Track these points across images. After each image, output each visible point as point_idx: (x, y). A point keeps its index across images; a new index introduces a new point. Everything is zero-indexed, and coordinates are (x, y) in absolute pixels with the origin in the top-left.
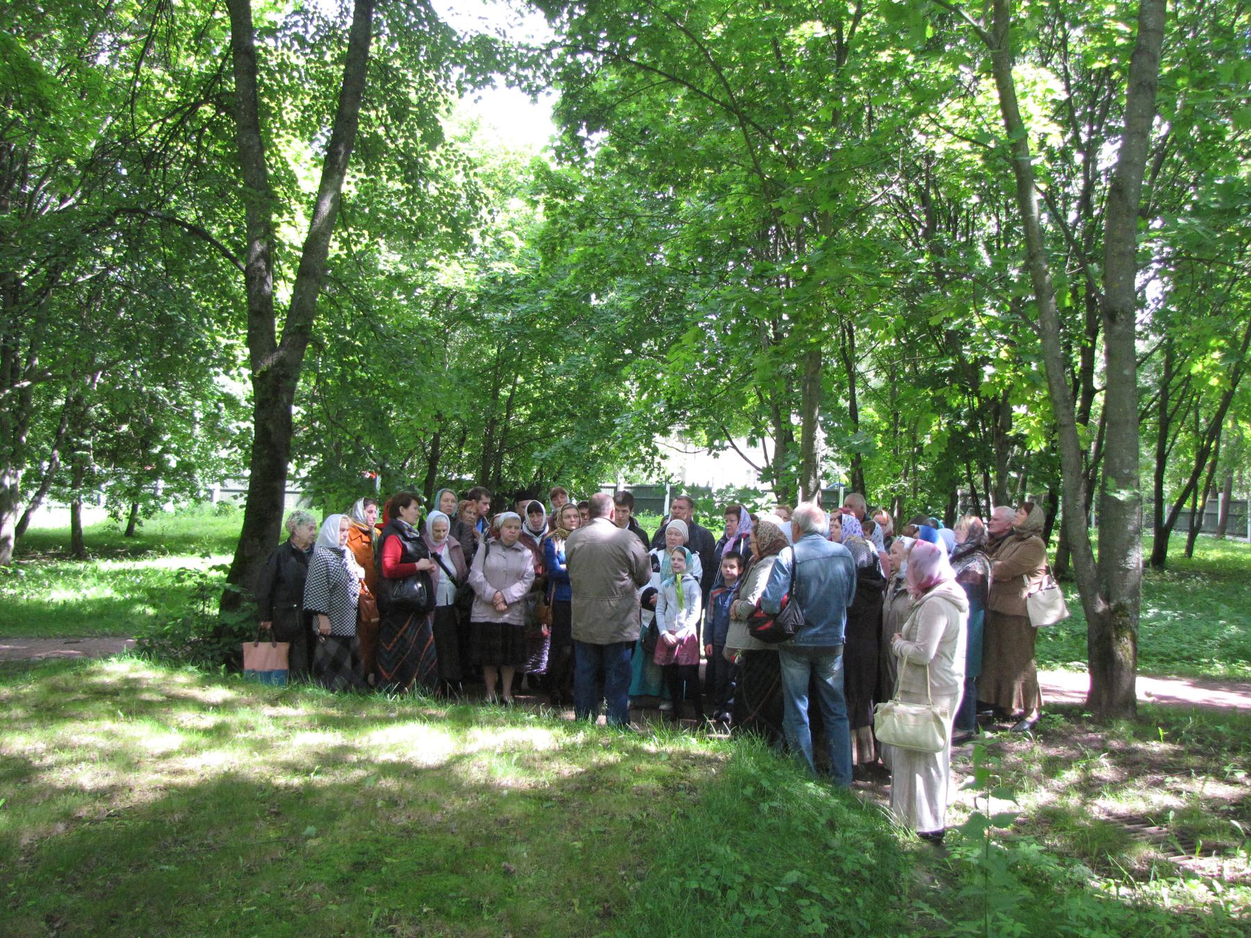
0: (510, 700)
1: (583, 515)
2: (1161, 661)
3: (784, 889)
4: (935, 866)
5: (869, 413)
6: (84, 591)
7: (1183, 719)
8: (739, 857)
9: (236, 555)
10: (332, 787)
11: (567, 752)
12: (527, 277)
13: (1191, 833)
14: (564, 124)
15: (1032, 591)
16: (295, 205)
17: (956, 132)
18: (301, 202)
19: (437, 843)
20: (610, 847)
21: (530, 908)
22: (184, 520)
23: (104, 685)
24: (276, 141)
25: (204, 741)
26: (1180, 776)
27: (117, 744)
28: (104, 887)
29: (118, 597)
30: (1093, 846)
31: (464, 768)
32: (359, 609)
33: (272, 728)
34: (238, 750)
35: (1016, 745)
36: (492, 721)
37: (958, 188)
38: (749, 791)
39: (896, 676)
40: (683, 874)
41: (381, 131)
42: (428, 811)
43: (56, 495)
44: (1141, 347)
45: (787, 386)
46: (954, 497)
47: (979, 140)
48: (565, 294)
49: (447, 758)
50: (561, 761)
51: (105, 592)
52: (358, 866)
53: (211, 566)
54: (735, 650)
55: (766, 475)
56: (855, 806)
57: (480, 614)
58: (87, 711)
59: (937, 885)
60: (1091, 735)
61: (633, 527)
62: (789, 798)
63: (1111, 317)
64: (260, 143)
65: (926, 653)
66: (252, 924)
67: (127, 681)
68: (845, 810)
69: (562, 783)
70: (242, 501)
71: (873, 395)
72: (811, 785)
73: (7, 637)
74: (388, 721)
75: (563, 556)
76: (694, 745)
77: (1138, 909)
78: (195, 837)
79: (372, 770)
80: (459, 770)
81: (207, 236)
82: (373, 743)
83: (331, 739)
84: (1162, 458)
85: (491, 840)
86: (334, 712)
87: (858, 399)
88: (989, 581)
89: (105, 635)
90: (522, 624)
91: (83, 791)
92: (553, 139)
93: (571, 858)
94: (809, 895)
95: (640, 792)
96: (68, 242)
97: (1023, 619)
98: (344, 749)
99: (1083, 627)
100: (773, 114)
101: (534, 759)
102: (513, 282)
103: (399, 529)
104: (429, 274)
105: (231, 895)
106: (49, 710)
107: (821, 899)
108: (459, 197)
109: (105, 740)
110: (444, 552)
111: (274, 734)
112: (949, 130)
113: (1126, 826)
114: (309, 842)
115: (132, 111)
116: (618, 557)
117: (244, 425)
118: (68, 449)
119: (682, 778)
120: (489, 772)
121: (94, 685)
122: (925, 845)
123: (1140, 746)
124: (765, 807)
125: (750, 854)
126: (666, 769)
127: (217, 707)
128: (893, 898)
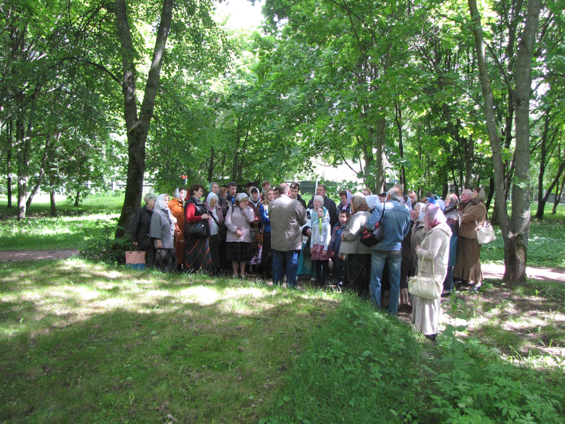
0: (243, 276)
1: (277, 193)
2: (538, 260)
3: (362, 359)
4: (432, 349)
5: (408, 148)
6: (57, 230)
7: (547, 286)
8: (342, 344)
9: (122, 213)
10: (163, 314)
11: (268, 299)
12: (252, 87)
13: (550, 337)
14: (267, 15)
15: (479, 228)
16: (144, 55)
17: (448, 17)
18: (147, 53)
19: (209, 338)
20: (286, 340)
21: (249, 366)
22: (100, 198)
23: (65, 270)
24: (135, 24)
25: (108, 294)
26: (544, 311)
27: (71, 296)
28: (66, 355)
29: (71, 233)
30: (503, 341)
31: (222, 305)
32: (175, 236)
33: (138, 288)
34: (123, 298)
35: (471, 297)
36: (235, 286)
37: (449, 44)
38: (348, 316)
39: (416, 265)
40: (318, 352)
41: (183, 20)
42: (205, 324)
43: (43, 189)
44: (533, 117)
45: (374, 135)
46: (446, 186)
47: (458, 20)
48: (269, 94)
49: (214, 301)
50: (265, 302)
51: (66, 230)
52: (174, 348)
53: (110, 219)
54: (343, 254)
55: (360, 175)
56: (397, 323)
57: (230, 238)
58: (57, 282)
59: (432, 358)
60: (505, 293)
61: (299, 199)
62: (366, 319)
63: (518, 102)
64: (128, 26)
65: (433, 255)
66: (128, 372)
67: (75, 268)
68: (392, 325)
69: (265, 312)
70: (124, 189)
71: (409, 139)
72: (377, 313)
73: (23, 250)
74: (189, 285)
75: (267, 212)
76: (325, 296)
77: (522, 369)
78: (104, 335)
79: (181, 306)
80: (220, 307)
81: (104, 69)
82: (182, 295)
83: (164, 293)
84: (542, 169)
85: (233, 336)
86: (165, 282)
87: (403, 141)
88: (460, 223)
89: (66, 249)
90: (250, 242)
91: (56, 315)
92: (262, 23)
93: (268, 345)
94: (374, 361)
95: (300, 316)
96: (44, 73)
97: (475, 241)
98: (169, 298)
99: (502, 245)
100: (363, 9)
101: (253, 302)
102: (246, 89)
103: (194, 201)
104: (207, 86)
105: (120, 360)
106: (41, 281)
107: (379, 363)
108: (220, 48)
109: (65, 294)
110: (214, 211)
111: (139, 292)
112: (444, 16)
113: (519, 333)
114: (154, 337)
115: (69, 12)
116: (291, 212)
117: (124, 156)
118: (47, 166)
119: (319, 310)
120: (233, 307)
121: (60, 270)
122: (428, 340)
123: (527, 298)
124: (355, 323)
125: (348, 344)
126: (311, 306)
127: (114, 280)
128: (412, 363)
